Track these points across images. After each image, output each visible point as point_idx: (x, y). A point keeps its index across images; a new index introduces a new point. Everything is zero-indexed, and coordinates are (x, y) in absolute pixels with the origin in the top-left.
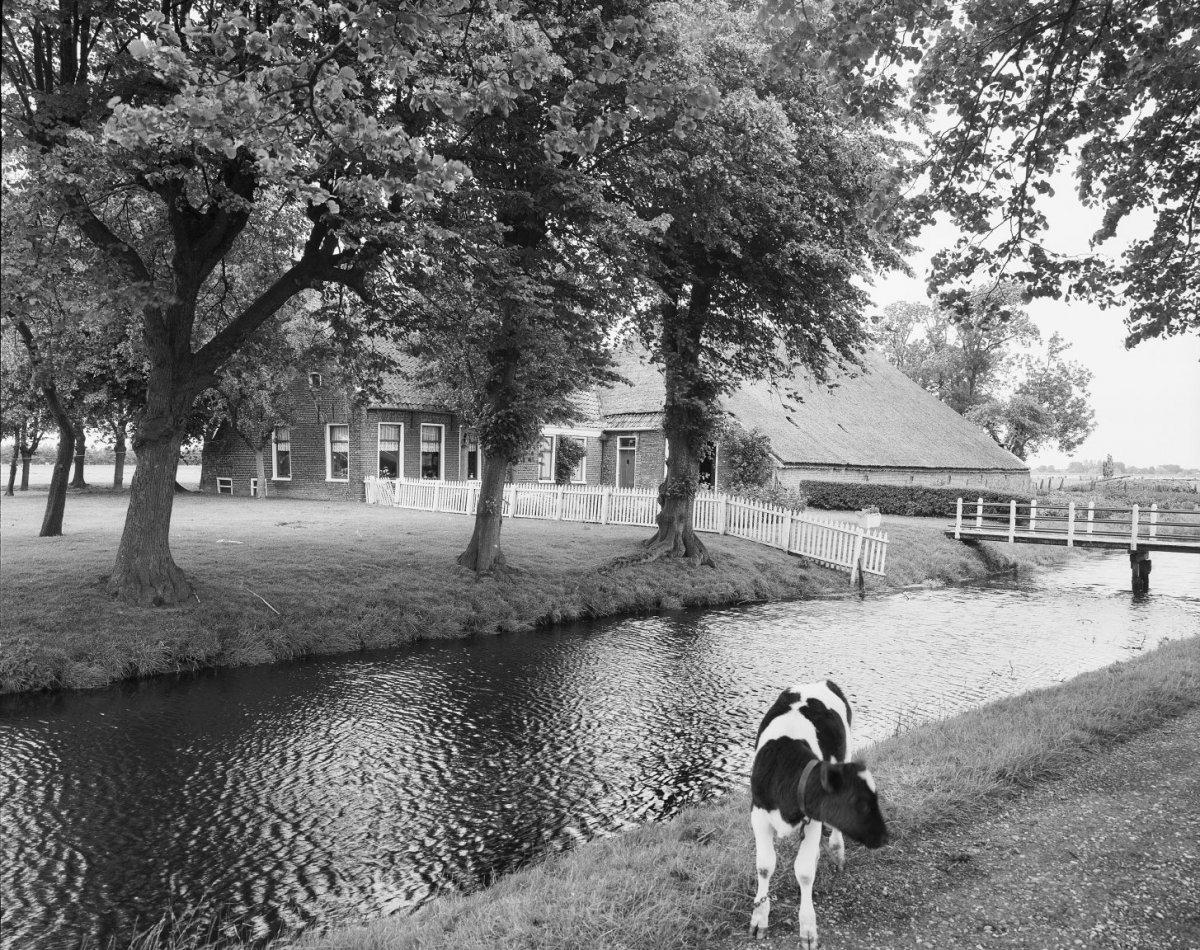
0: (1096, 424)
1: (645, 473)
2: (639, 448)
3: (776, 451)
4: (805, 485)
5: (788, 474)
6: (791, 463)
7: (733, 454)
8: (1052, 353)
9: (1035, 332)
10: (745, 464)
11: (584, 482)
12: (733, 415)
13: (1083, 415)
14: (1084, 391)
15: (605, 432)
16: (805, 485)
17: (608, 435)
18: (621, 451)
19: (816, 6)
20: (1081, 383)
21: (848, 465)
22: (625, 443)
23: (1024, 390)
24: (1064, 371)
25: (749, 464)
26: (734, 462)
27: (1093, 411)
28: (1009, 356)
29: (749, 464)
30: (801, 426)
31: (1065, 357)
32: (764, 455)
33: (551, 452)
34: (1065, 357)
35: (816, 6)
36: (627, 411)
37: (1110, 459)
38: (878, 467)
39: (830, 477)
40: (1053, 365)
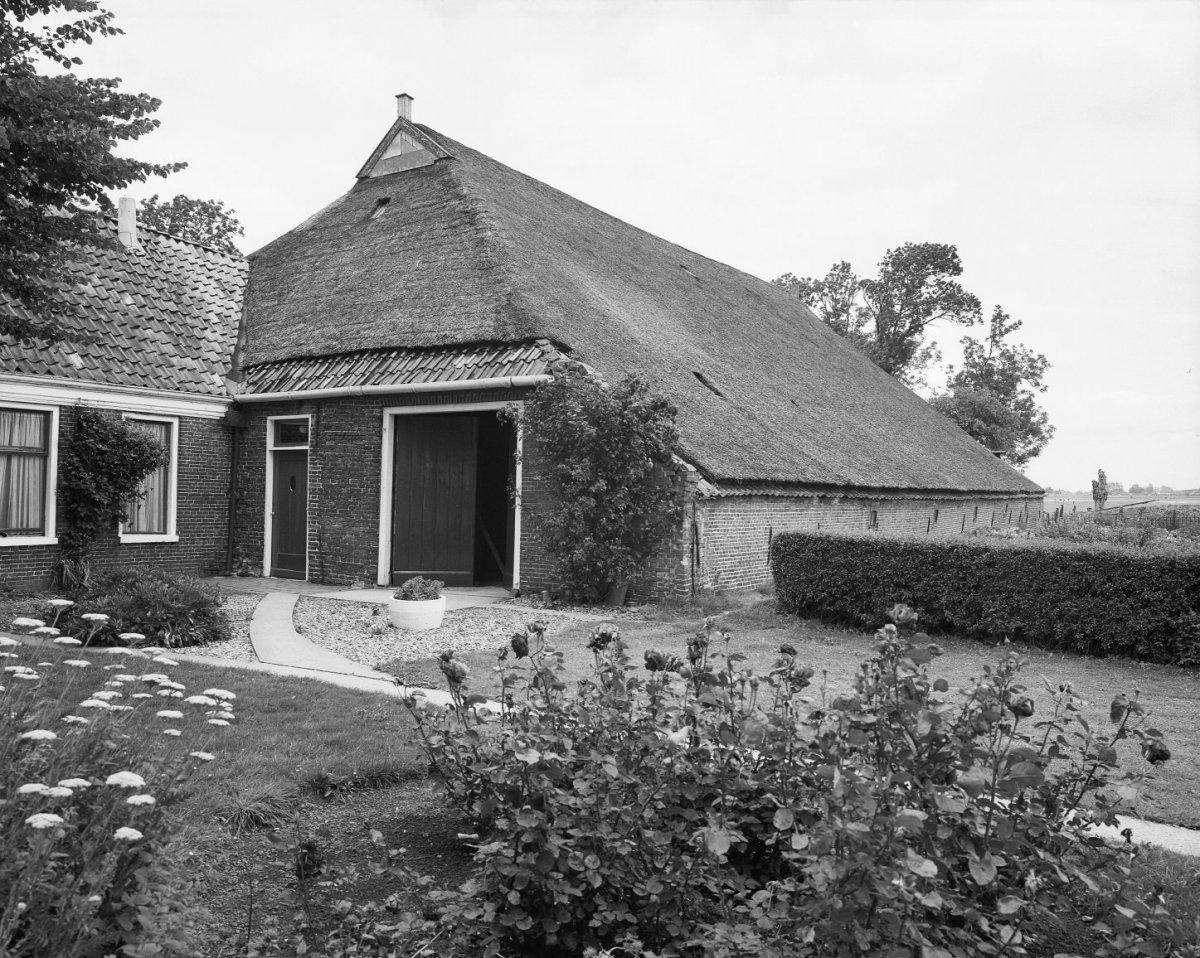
0: (1052, 428)
1: (331, 512)
2: (316, 446)
3: (688, 447)
4: (787, 551)
5: (723, 512)
6: (730, 483)
7: (562, 457)
8: (994, 339)
9: (974, 303)
10: (602, 484)
11: (156, 530)
12: (564, 348)
13: (1033, 419)
14: (1037, 384)
15: (237, 407)
16: (787, 551)
17: (242, 419)
18: (275, 453)
19: (403, 955)
20: (1034, 374)
21: (849, 487)
22: (286, 433)
23: (959, 382)
24: (1010, 358)
25: (614, 485)
26: (567, 478)
27: (1045, 414)
28: (923, 346)
29: (614, 485)
30: (729, 395)
31: (1010, 341)
32: (661, 459)
33: (44, 455)
34: (1010, 341)
35: (403, 955)
36: (296, 351)
37: (1102, 476)
38: (895, 490)
39: (843, 523)
40: (996, 353)
